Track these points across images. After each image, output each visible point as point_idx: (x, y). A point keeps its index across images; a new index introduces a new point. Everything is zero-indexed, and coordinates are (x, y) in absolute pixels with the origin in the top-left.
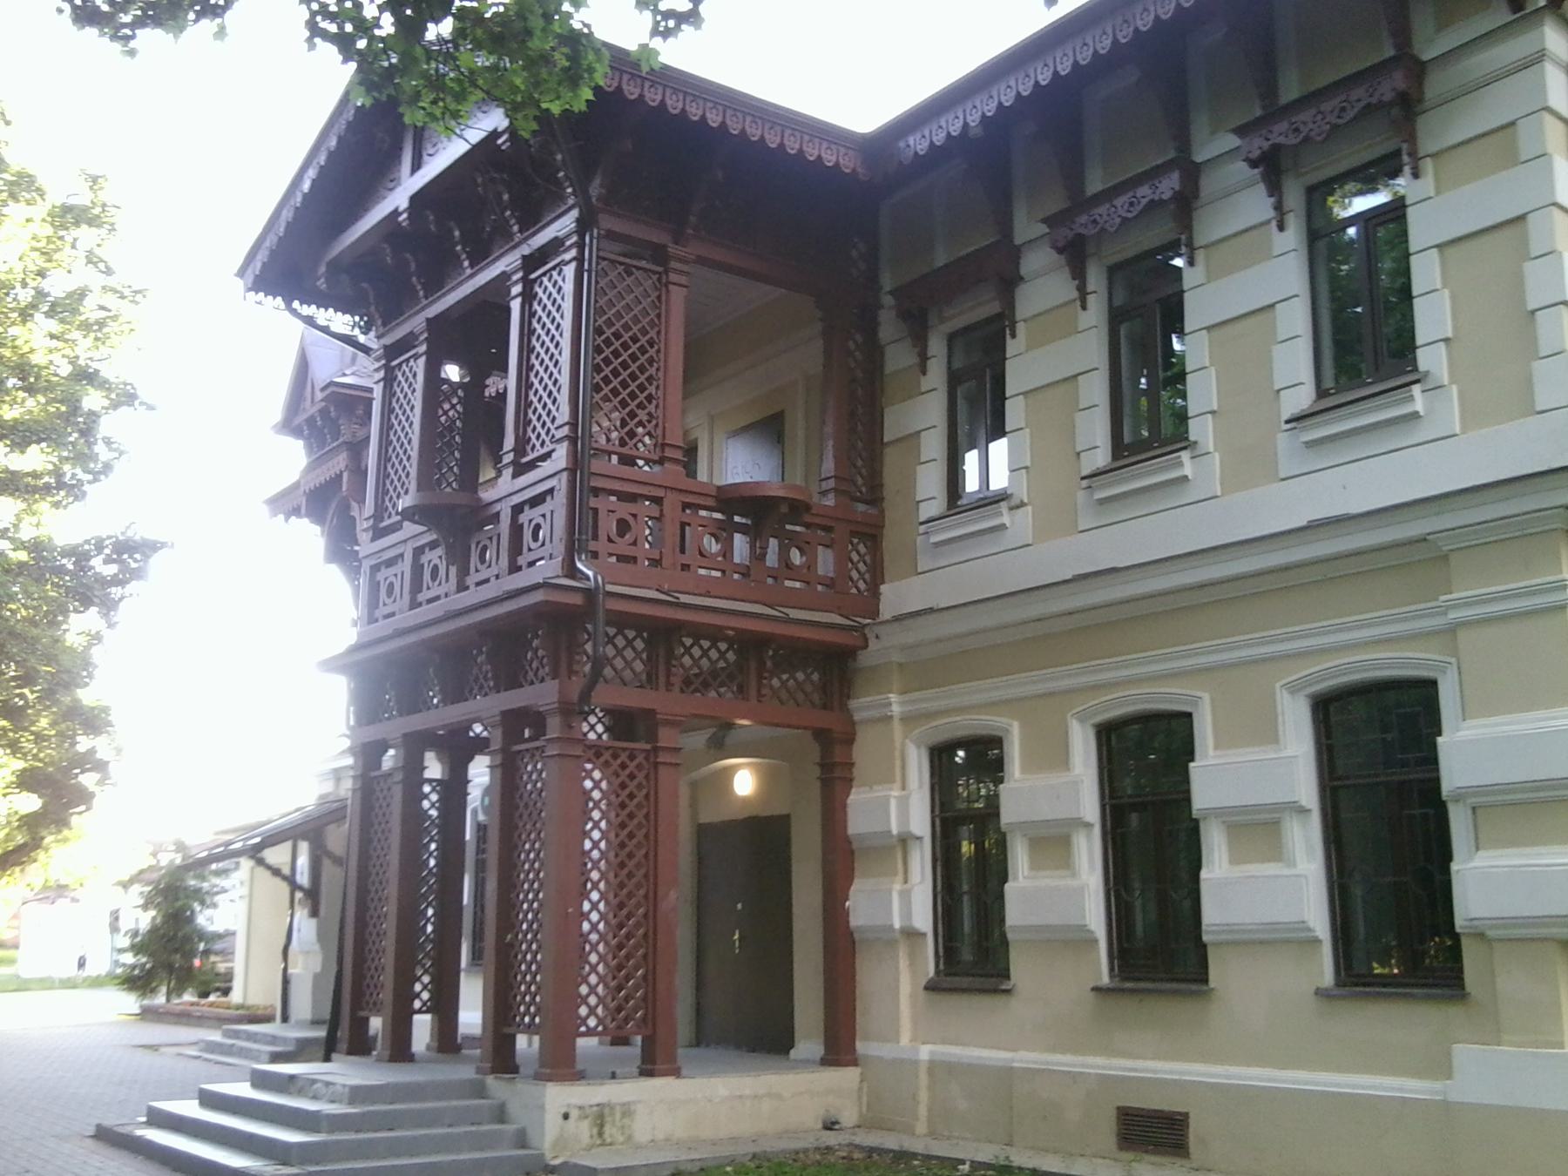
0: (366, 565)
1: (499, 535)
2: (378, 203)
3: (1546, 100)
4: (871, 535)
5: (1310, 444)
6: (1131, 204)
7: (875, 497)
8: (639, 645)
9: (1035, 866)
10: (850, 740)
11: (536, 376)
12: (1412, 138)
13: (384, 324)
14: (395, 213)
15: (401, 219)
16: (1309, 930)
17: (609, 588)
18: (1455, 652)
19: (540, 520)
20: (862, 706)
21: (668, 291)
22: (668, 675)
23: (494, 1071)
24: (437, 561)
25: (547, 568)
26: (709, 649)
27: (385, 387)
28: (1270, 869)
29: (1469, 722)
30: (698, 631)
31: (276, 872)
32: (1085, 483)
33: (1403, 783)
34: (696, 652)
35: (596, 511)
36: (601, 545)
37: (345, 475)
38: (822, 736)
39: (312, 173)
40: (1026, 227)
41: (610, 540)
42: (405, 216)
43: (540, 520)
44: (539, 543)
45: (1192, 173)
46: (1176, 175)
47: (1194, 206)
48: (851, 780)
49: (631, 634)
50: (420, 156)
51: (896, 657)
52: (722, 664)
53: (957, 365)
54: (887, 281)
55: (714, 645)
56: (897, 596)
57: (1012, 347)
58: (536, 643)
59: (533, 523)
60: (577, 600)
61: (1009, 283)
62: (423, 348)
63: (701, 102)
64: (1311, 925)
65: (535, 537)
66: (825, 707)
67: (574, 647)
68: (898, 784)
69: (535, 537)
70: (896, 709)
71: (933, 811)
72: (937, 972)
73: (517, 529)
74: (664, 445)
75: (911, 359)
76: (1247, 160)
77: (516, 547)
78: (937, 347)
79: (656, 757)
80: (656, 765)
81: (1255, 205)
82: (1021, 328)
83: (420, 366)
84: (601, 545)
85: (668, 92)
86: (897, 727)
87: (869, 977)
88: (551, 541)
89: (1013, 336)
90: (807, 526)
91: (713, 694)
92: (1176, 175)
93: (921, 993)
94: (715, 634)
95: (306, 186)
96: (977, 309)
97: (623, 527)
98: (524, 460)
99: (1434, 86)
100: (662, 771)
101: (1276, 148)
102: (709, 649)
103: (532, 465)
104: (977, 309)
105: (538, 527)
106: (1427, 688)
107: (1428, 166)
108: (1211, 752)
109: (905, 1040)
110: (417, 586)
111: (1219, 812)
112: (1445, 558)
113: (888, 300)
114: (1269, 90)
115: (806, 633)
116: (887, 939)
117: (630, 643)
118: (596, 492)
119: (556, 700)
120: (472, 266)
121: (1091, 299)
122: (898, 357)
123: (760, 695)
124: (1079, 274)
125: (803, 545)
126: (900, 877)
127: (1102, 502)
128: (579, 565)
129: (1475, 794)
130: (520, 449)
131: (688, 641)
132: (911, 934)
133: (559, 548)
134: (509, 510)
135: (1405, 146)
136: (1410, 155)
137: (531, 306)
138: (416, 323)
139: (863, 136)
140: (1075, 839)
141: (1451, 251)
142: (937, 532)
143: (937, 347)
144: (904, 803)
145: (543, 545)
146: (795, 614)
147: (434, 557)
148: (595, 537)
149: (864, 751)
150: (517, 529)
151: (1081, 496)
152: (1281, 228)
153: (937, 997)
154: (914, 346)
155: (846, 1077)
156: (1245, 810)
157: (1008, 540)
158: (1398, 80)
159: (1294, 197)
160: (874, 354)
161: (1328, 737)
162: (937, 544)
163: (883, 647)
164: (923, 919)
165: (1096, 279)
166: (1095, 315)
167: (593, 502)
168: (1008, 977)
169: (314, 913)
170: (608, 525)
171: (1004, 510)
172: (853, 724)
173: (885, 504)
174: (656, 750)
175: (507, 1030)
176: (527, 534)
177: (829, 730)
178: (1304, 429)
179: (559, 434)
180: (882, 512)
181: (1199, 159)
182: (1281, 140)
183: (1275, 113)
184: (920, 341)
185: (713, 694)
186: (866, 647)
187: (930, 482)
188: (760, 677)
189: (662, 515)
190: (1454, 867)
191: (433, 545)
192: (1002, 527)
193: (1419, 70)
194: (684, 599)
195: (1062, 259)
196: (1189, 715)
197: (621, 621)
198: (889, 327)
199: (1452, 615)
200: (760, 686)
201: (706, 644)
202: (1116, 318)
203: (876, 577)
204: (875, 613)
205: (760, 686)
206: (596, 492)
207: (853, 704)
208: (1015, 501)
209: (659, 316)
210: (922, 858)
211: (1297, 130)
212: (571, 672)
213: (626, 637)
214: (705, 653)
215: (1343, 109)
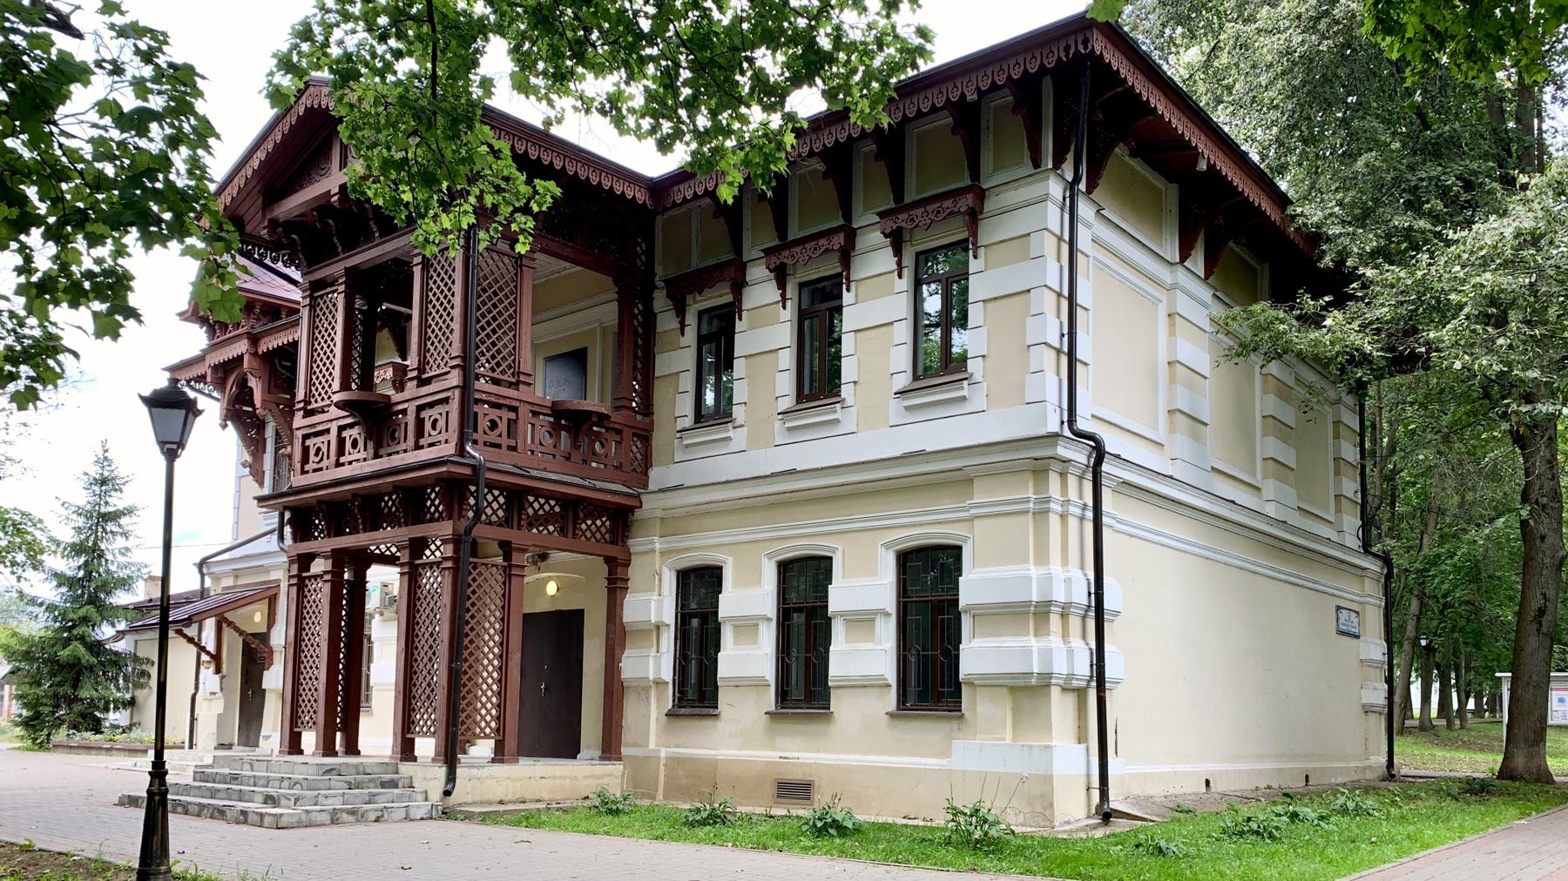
0: (299, 434)
1: (406, 424)
2: (311, 183)
3: (1046, 224)
4: (645, 437)
5: (907, 408)
6: (815, 249)
7: (647, 408)
8: (501, 500)
9: (737, 642)
10: (627, 564)
11: (433, 320)
12: (975, 234)
13: (309, 266)
14: (328, 194)
15: (332, 200)
16: (886, 679)
17: (489, 465)
18: (972, 533)
19: (438, 417)
20: (636, 544)
21: (522, 271)
22: (520, 519)
23: (402, 760)
24: (358, 437)
25: (448, 450)
26: (499, 496)
27: (310, 310)
28: (868, 646)
29: (976, 570)
30: (538, 493)
31: (191, 640)
32: (780, 417)
33: (939, 601)
34: (536, 506)
35: (476, 414)
36: (479, 436)
37: (246, 358)
38: (609, 560)
39: (261, 155)
40: (751, 251)
41: (485, 433)
42: (336, 198)
43: (438, 417)
44: (437, 432)
45: (851, 235)
46: (842, 236)
47: (852, 254)
48: (627, 588)
49: (496, 493)
50: (346, 157)
51: (659, 514)
52: (541, 512)
53: (704, 332)
54: (659, 271)
55: (547, 502)
56: (658, 477)
57: (739, 326)
58: (433, 496)
59: (432, 418)
60: (467, 471)
61: (739, 286)
62: (341, 288)
63: (550, 152)
64: (886, 676)
65: (434, 426)
66: (612, 543)
67: (463, 500)
68: (656, 593)
69: (434, 426)
70: (657, 546)
71: (677, 609)
72: (673, 706)
73: (420, 423)
74: (519, 373)
75: (675, 324)
76: (883, 233)
77: (420, 432)
78: (691, 319)
79: (510, 570)
80: (510, 575)
81: (884, 260)
82: (744, 314)
83: (341, 301)
84: (479, 436)
85: (529, 144)
86: (657, 554)
87: (631, 711)
88: (447, 431)
89: (740, 319)
90: (607, 429)
91: (535, 531)
92: (842, 236)
93: (664, 718)
94: (549, 496)
95: (255, 163)
96: (718, 296)
97: (494, 425)
98: (424, 376)
99: (989, 206)
100: (514, 579)
101: (900, 229)
102: (499, 496)
103: (428, 381)
104: (718, 296)
105: (435, 421)
106: (956, 551)
107: (981, 251)
108: (840, 579)
109: (652, 746)
110: (341, 451)
111: (842, 614)
112: (971, 480)
113: (660, 284)
114: (898, 193)
115: (608, 498)
116: (644, 687)
117: (496, 499)
118: (477, 401)
119: (451, 532)
120: (381, 236)
121: (789, 303)
122: (666, 322)
123: (574, 534)
124: (782, 285)
125: (605, 442)
126: (655, 649)
127: (789, 429)
128: (468, 449)
129: (974, 609)
130: (421, 369)
131: (531, 499)
132: (659, 683)
133: (454, 437)
134: (415, 408)
135: (971, 239)
136: (973, 244)
137: (428, 272)
138: (336, 269)
139: (651, 179)
140: (760, 627)
141: (990, 305)
142: (687, 438)
143: (691, 319)
144: (660, 603)
145: (440, 433)
146: (599, 484)
147: (354, 432)
148: (476, 430)
149: (635, 573)
150: (420, 423)
151: (777, 424)
152: (900, 276)
153: (673, 720)
154: (678, 317)
155: (615, 768)
156: (857, 612)
157: (733, 447)
158: (967, 201)
159: (908, 260)
160: (650, 319)
161: (904, 574)
162: (687, 446)
163: (651, 505)
164: (667, 674)
165: (791, 291)
166: (788, 314)
167: (476, 408)
168: (717, 707)
169: (218, 670)
170: (483, 423)
171: (731, 428)
172: (630, 554)
173: (655, 417)
174: (510, 566)
175: (409, 736)
176: (428, 425)
177: (510, 543)
178: (907, 399)
179: (454, 362)
180: (652, 422)
181: (855, 226)
182: (903, 224)
183: (901, 207)
184: (681, 312)
185: (535, 531)
186: (641, 507)
187: (686, 406)
188: (575, 523)
189: (517, 418)
190: (961, 647)
191: (351, 426)
192: (729, 439)
193: (981, 195)
194: (534, 473)
195: (772, 275)
196: (831, 558)
197: (491, 485)
198: (660, 301)
199: (972, 511)
200: (574, 528)
201: (542, 501)
202: (802, 316)
203: (647, 463)
204: (646, 486)
205: (574, 528)
206: (477, 401)
207: (630, 542)
208: (737, 423)
209: (516, 287)
210: (669, 638)
211: (912, 220)
212: (461, 516)
213: (493, 495)
214: (542, 506)
215: (939, 212)
